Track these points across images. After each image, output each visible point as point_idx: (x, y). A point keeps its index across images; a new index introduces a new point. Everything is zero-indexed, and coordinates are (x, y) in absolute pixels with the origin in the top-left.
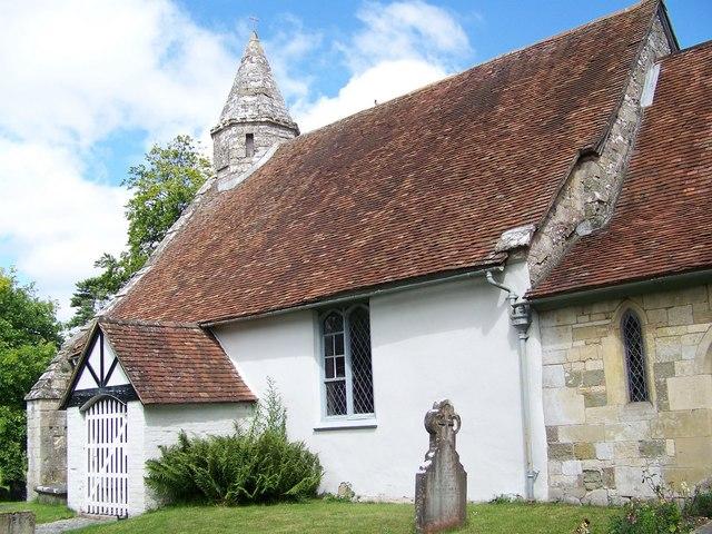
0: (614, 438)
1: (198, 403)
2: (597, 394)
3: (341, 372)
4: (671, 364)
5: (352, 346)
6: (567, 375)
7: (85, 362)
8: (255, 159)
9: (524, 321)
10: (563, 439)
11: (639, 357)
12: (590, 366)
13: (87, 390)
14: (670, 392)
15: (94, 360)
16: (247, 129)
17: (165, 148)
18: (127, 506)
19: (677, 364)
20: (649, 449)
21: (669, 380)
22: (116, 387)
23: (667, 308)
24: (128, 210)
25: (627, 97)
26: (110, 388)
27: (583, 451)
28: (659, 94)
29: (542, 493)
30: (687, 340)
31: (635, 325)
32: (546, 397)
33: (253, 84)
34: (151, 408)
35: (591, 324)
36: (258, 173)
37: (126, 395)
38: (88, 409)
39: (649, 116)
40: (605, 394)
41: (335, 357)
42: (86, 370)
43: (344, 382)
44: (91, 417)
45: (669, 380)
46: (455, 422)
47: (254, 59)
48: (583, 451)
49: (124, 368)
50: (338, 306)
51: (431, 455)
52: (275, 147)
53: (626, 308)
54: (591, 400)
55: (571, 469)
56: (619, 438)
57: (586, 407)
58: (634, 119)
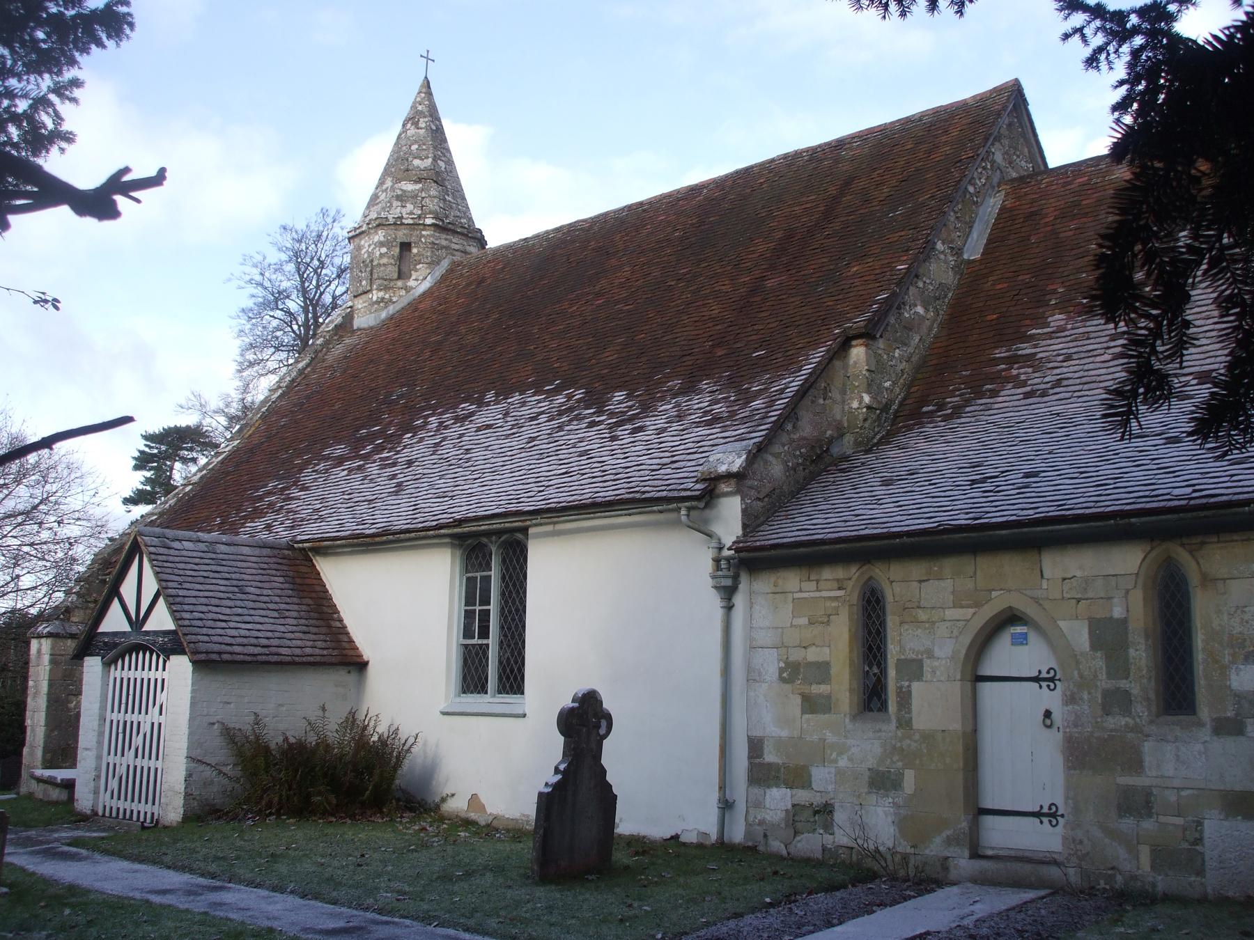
0: (836, 761)
1: (276, 663)
2: (820, 696)
3: (484, 633)
4: (920, 663)
5: (503, 594)
6: (782, 665)
7: (115, 592)
8: (411, 283)
9: (728, 582)
10: (770, 757)
11: (879, 648)
12: (813, 655)
13: (115, 634)
14: (916, 703)
15: (128, 588)
16: (402, 235)
17: (300, 226)
18: (156, 809)
19: (927, 662)
20: (882, 782)
21: (916, 686)
22: (156, 633)
23: (920, 581)
24: (234, 322)
25: (940, 246)
26: (147, 633)
27: (796, 777)
28: (993, 243)
29: (737, 834)
30: (942, 629)
31: (878, 601)
32: (752, 694)
33: (417, 162)
34: (205, 664)
35: (817, 594)
36: (414, 306)
37: (171, 645)
38: (116, 662)
39: (972, 275)
40: (829, 697)
41: (478, 608)
42: (116, 602)
43: (487, 645)
44: (116, 673)
45: (916, 686)
46: (604, 723)
47: (422, 125)
48: (796, 777)
49: (170, 605)
50: (488, 534)
51: (562, 767)
52: (445, 264)
53: (866, 577)
54: (811, 705)
55: (778, 800)
56: (843, 762)
57: (803, 712)
58: (950, 278)
